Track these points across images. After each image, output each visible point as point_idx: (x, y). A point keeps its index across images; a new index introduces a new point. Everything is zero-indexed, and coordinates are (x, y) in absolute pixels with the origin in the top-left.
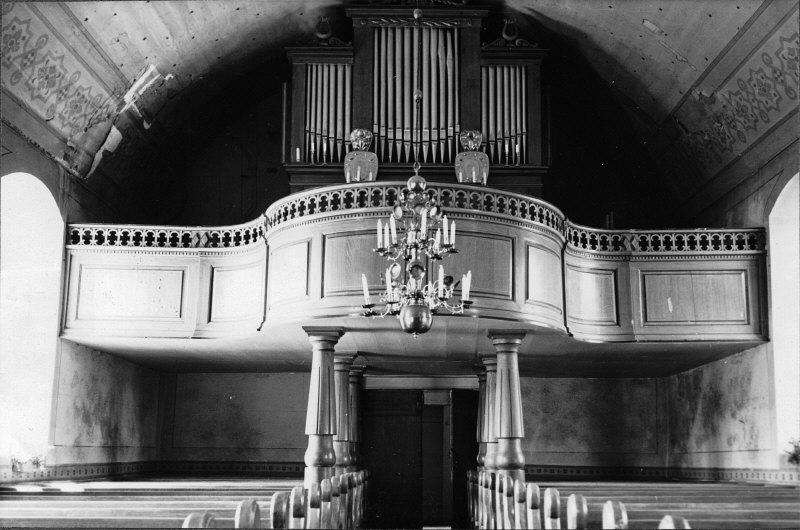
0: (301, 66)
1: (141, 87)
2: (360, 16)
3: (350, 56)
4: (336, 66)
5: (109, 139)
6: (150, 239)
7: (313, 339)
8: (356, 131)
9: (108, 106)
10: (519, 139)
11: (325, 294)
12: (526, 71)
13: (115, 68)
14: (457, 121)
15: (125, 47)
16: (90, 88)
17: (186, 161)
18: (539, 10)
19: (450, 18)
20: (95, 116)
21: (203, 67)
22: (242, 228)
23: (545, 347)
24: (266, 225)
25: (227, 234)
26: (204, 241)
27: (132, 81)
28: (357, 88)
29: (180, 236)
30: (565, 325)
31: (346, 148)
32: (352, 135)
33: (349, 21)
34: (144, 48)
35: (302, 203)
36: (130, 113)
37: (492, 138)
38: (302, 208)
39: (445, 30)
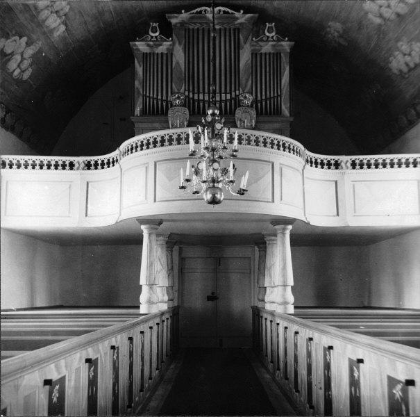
6: (96, 165)
7: (143, 227)
11: (157, 200)
17: (73, 112)
22: (105, 157)
23: (303, 230)
24: (120, 156)
25: (96, 162)
26: (82, 165)
29: (67, 163)
30: (305, 215)
31: (169, 104)
35: (148, 140)
37: (259, 98)
38: (148, 144)
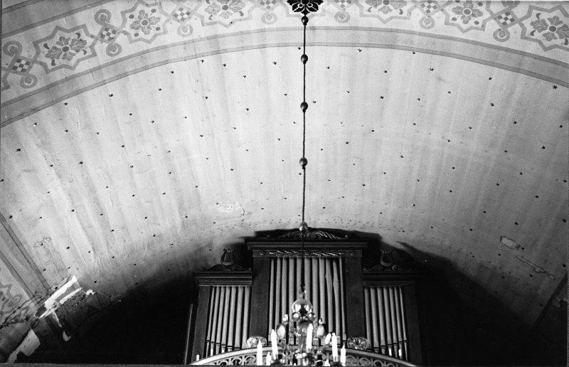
0: (207, 288)
1: (62, 296)
2: (259, 248)
3: (250, 279)
4: (237, 288)
5: (25, 342)
8: (250, 339)
9: (27, 308)
10: (400, 346)
12: (402, 290)
13: (38, 272)
14: (344, 331)
15: (48, 252)
16: (9, 286)
18: (410, 244)
19: (335, 250)
20: (13, 316)
21: (122, 289)
27: (53, 289)
28: (255, 305)
32: (248, 341)
33: (251, 253)
34: (67, 257)
36: (49, 318)
39: (331, 260)
